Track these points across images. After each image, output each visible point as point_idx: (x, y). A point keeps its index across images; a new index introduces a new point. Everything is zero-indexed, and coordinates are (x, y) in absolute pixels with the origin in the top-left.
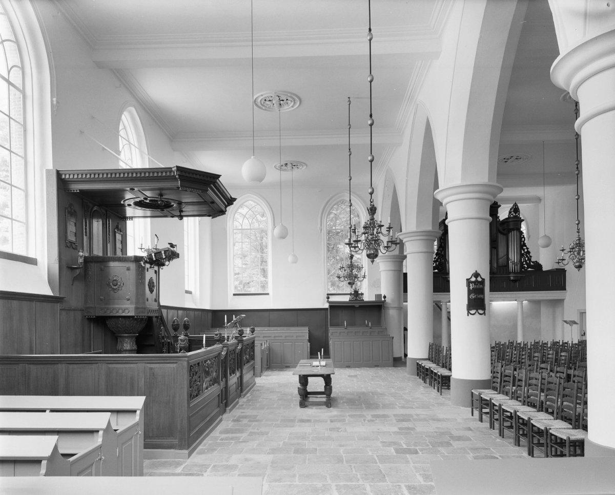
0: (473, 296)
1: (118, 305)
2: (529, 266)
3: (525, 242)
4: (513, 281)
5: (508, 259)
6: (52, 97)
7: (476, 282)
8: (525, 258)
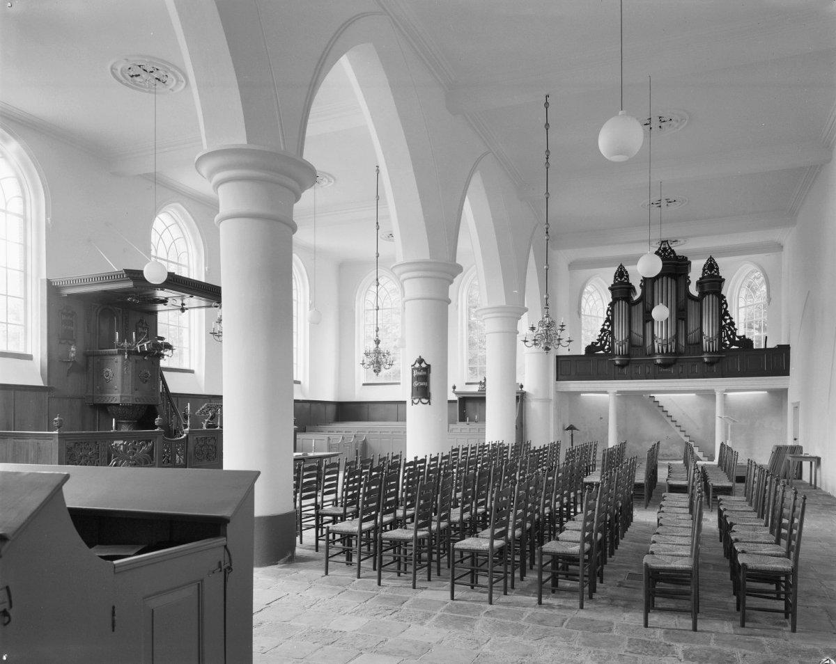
0: (416, 384)
1: (109, 393)
2: (733, 342)
5: (701, 333)
6: (47, 216)
7: (419, 369)
8: (727, 332)
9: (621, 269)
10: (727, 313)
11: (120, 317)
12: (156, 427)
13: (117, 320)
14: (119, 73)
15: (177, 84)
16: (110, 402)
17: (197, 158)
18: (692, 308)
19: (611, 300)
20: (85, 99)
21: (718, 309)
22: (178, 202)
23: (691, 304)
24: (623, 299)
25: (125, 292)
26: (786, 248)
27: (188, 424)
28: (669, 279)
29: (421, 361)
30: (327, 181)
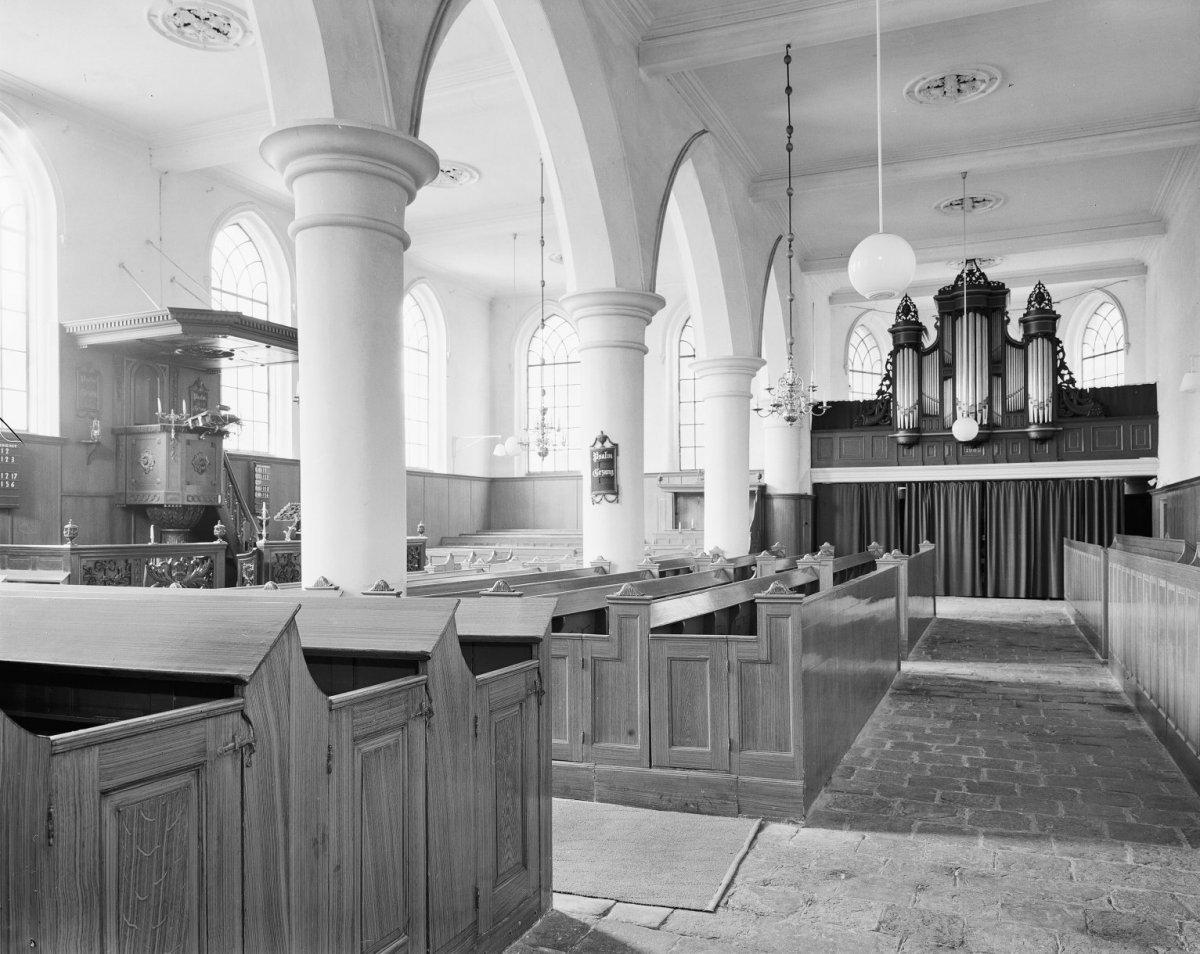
0: (597, 473)
3: (1065, 360)
4: (1036, 440)
9: (906, 301)
10: (1063, 366)
11: (166, 379)
12: (215, 539)
13: (162, 383)
14: (159, 22)
15: (244, 36)
16: (149, 502)
17: (261, 140)
18: (1013, 357)
19: (892, 348)
20: (126, 63)
21: (1051, 359)
22: (253, 210)
23: (1011, 352)
24: (910, 346)
25: (172, 342)
26: (1152, 271)
27: (264, 533)
28: (978, 316)
29: (604, 439)
30: (469, 176)
